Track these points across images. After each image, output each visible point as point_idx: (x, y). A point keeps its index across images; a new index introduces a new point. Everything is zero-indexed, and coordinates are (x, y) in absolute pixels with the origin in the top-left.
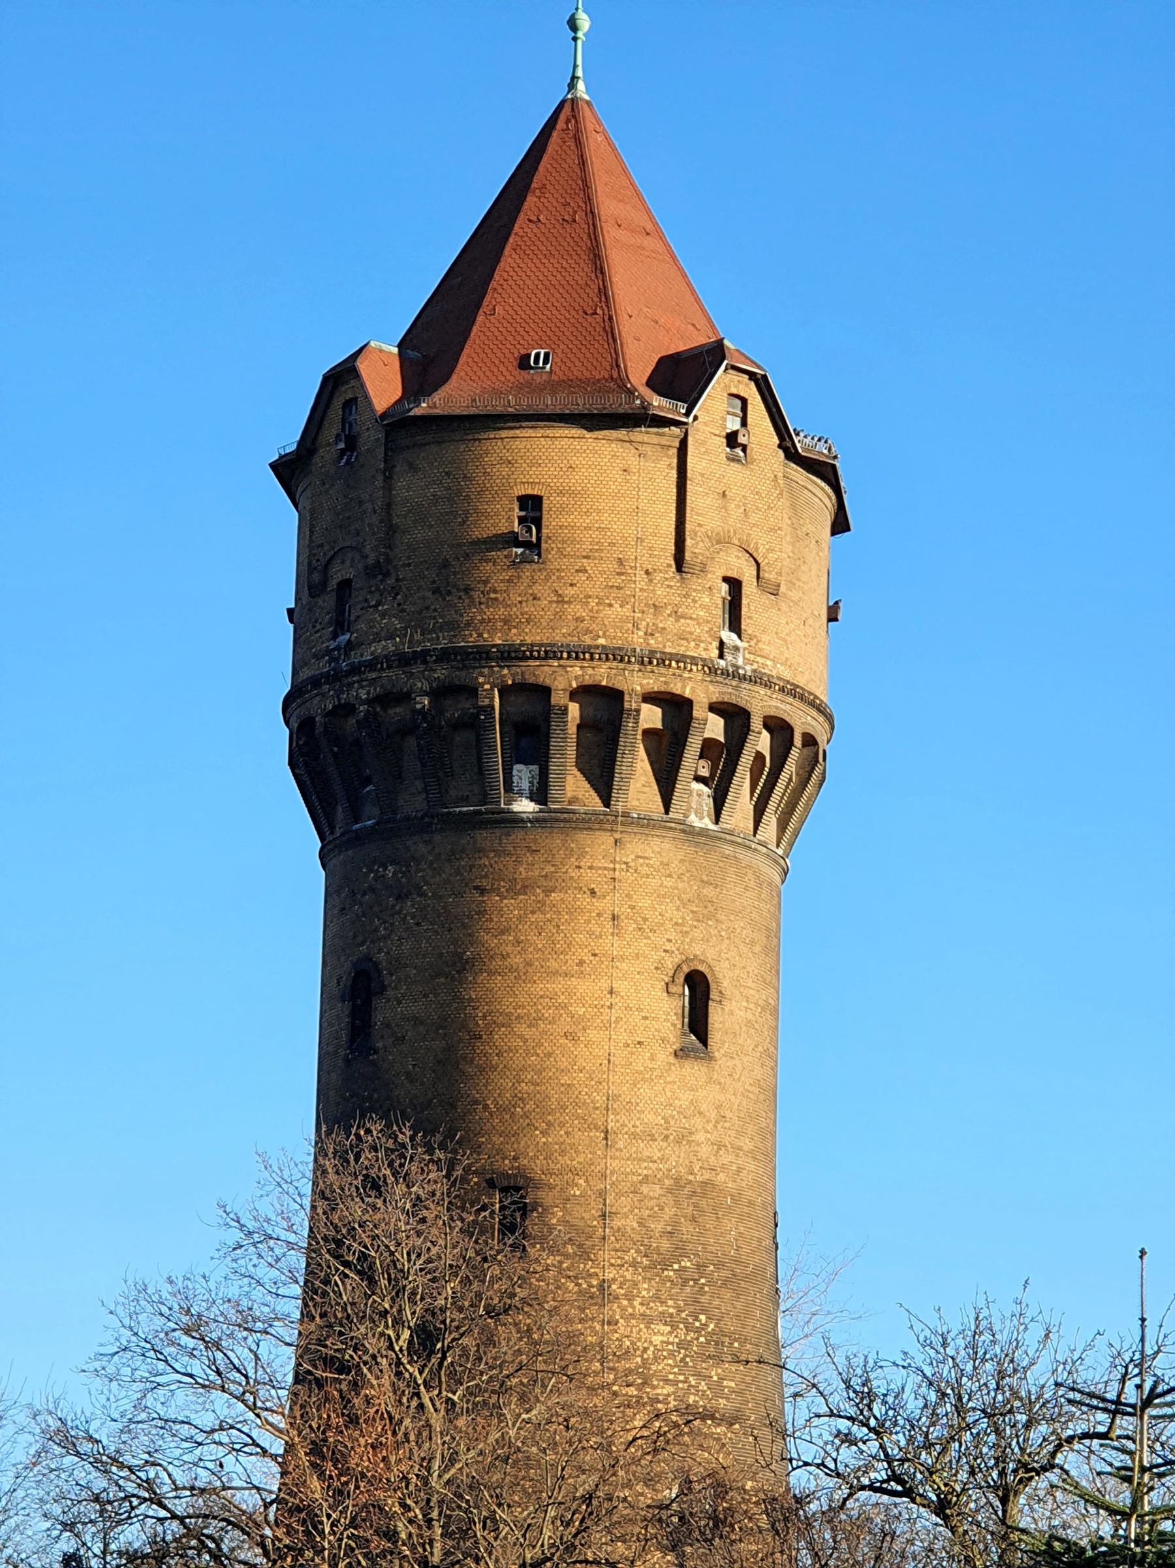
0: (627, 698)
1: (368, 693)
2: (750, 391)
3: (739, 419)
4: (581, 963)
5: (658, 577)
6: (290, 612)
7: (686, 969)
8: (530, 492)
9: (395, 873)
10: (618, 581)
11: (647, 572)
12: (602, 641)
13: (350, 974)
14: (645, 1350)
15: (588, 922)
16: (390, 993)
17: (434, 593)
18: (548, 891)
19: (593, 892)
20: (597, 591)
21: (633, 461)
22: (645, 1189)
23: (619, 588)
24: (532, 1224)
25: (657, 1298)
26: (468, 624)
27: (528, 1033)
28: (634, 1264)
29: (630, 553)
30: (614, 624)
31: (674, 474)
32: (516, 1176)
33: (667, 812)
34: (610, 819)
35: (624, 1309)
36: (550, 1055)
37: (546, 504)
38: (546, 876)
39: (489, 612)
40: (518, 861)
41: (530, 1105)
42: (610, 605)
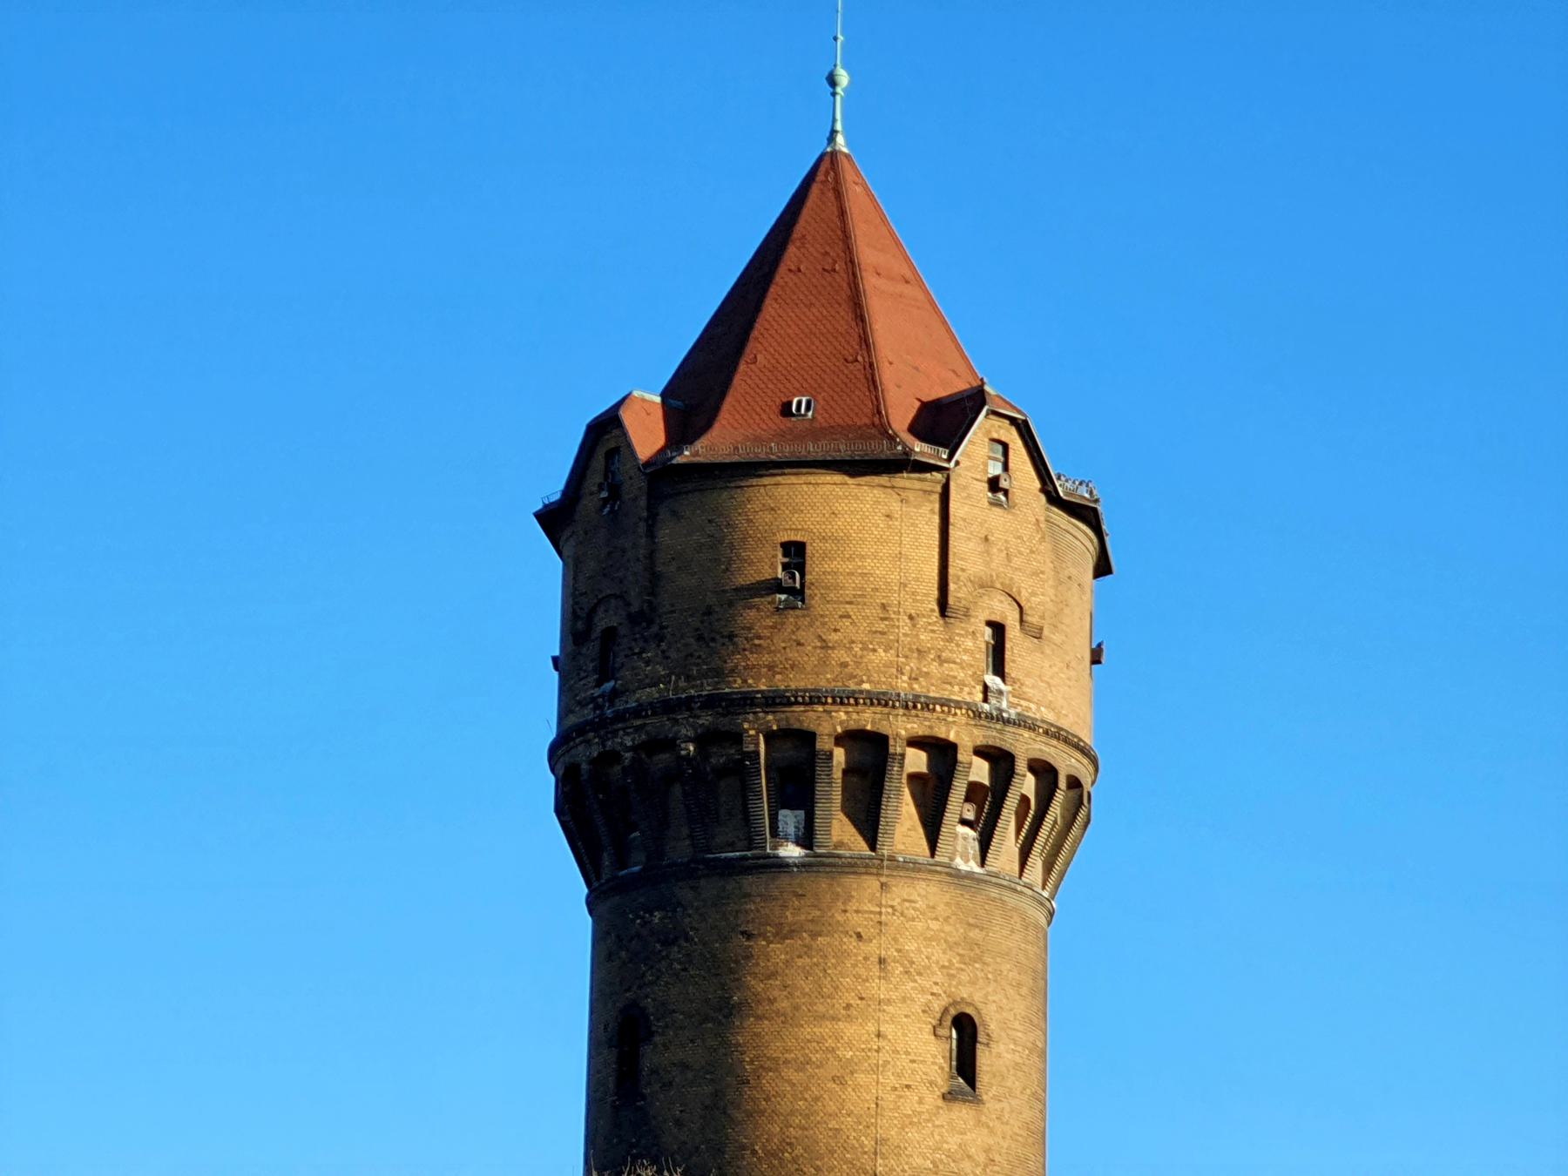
0: (891, 742)
3: (936, 497)
4: (848, 1006)
5: (922, 622)
6: (555, 660)
7: (953, 1012)
10: (882, 626)
11: (911, 617)
12: (866, 686)
15: (855, 966)
16: (657, 1039)
18: (815, 935)
19: (859, 936)
27: (795, 1077)
31: (936, 519)
33: (933, 855)
36: (816, 1099)
37: (809, 550)
40: (784, 907)
41: (799, 1150)
42: (874, 650)
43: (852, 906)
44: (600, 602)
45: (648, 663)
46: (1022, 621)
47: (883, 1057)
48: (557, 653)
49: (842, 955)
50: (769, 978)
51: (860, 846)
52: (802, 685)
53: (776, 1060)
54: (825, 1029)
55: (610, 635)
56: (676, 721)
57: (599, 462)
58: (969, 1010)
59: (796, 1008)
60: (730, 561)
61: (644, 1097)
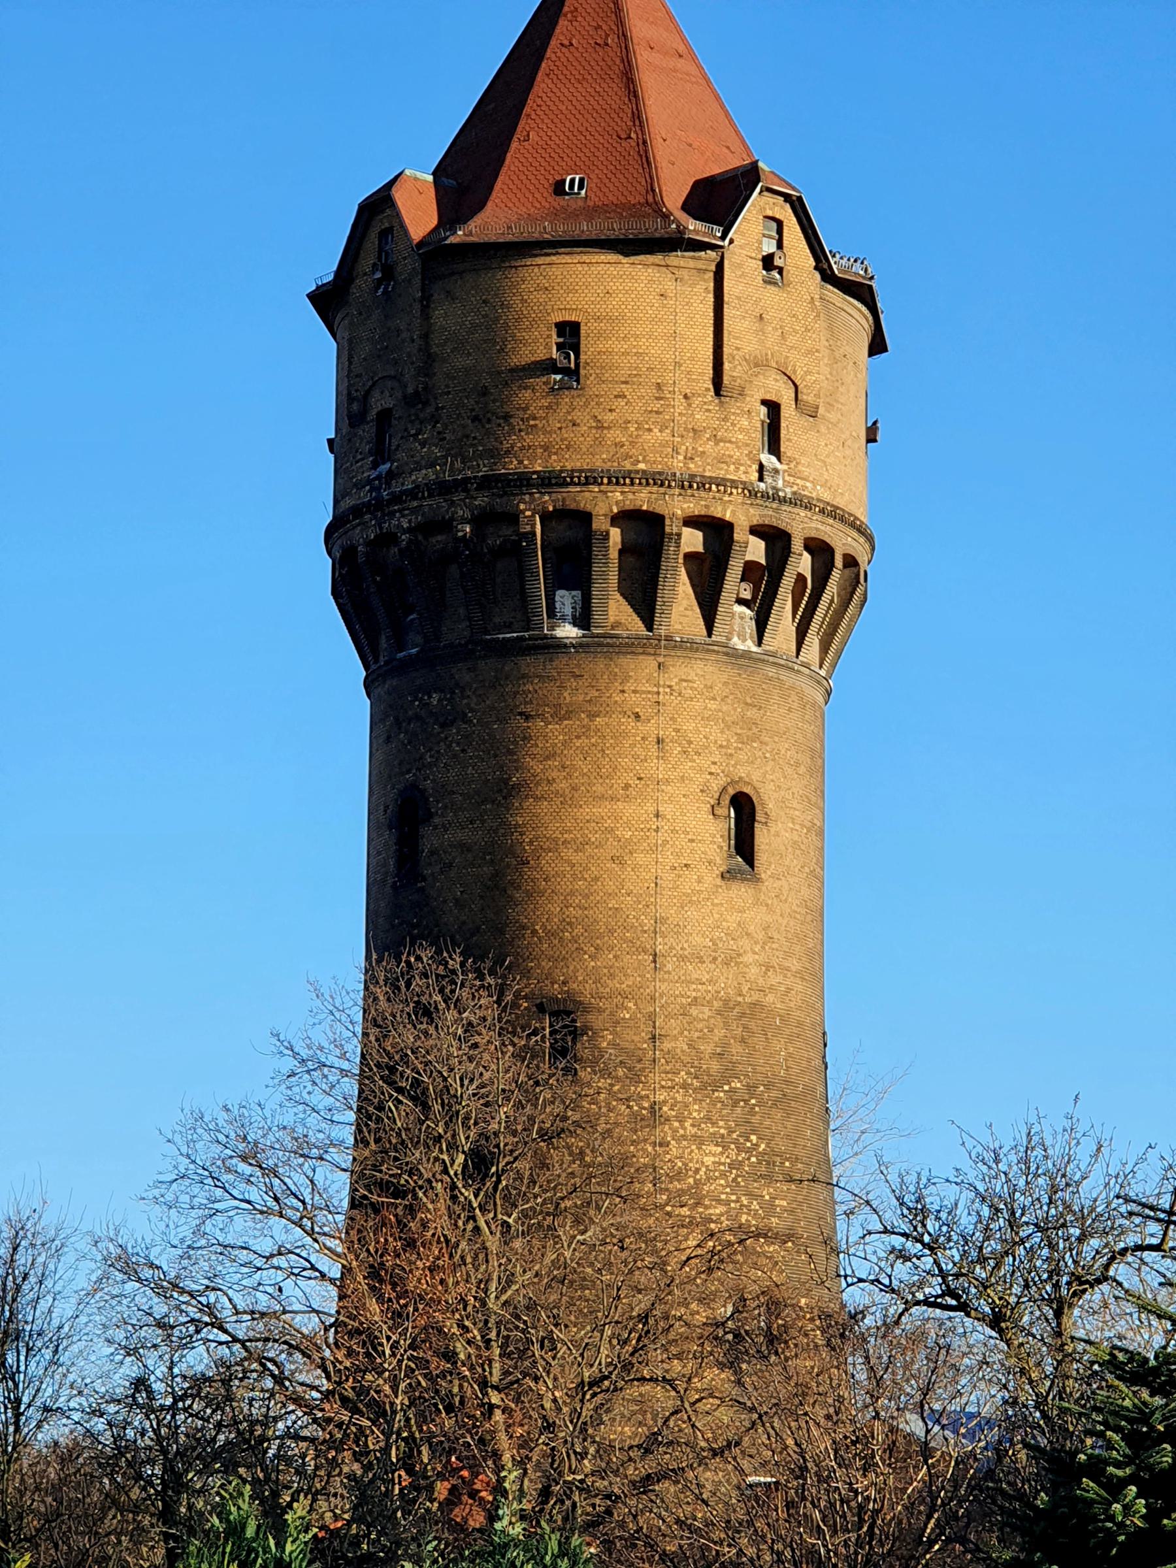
0: (667, 522)
1: (410, 522)
3: (775, 242)
4: (627, 787)
5: (697, 401)
6: (331, 442)
8: (567, 318)
10: (657, 406)
11: (686, 397)
12: (642, 466)
14: (697, 1171)
15: (633, 746)
18: (592, 716)
19: (637, 716)
23: (657, 412)
24: (583, 1048)
26: (508, 452)
27: (576, 858)
28: (685, 1086)
29: (669, 378)
30: (655, 448)
33: (710, 635)
35: (675, 1131)
36: (596, 879)
41: (579, 930)
42: (650, 430)
45: (423, 444)
50: (548, 758)
51: (636, 625)
58: (747, 790)
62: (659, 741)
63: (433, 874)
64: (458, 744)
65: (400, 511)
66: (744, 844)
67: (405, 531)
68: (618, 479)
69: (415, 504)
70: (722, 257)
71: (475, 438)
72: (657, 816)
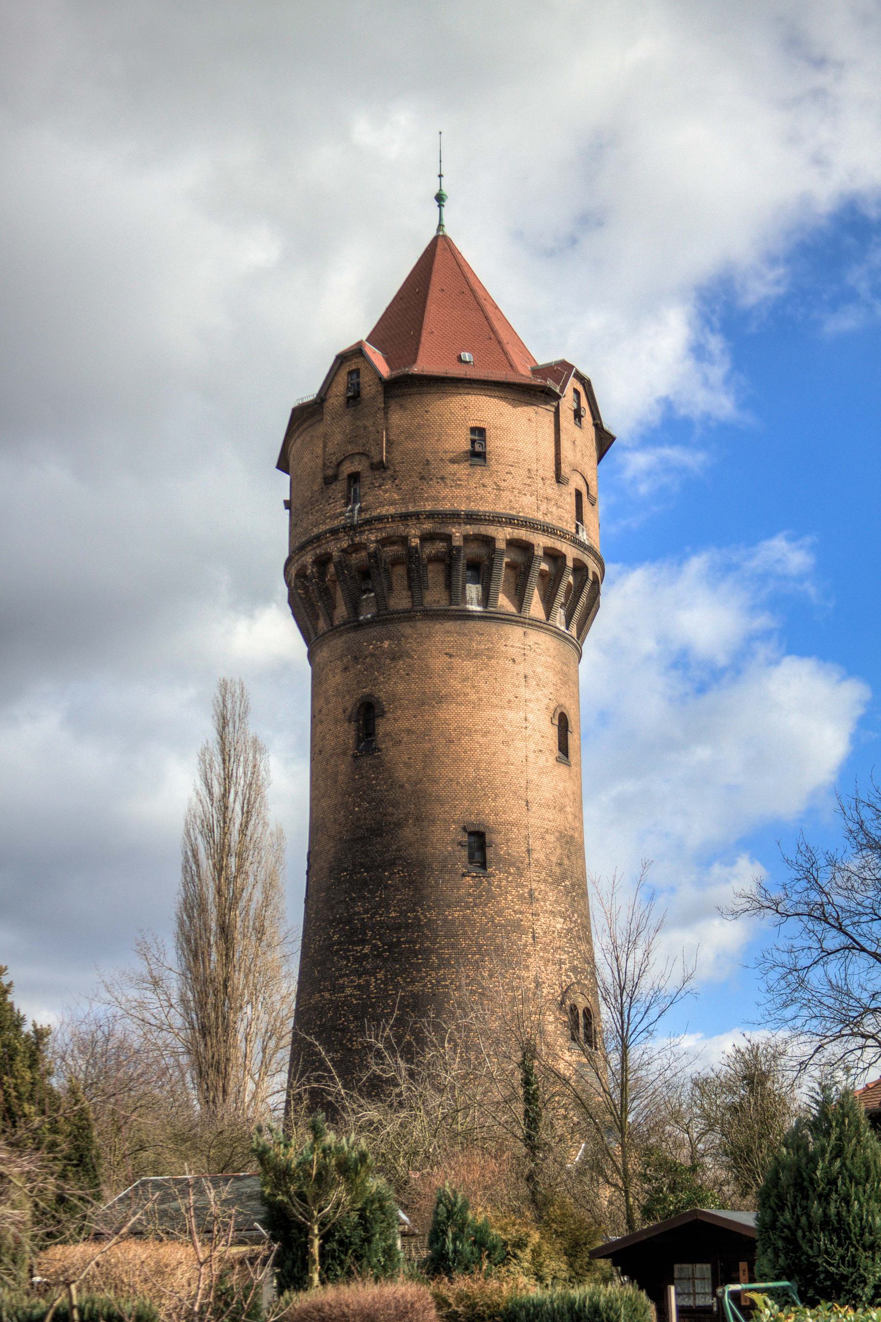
0: (536, 548)
1: (376, 537)
2: (580, 389)
3: (552, 414)
4: (509, 701)
5: (548, 482)
6: (286, 502)
7: (559, 711)
8: (478, 425)
9: (389, 645)
10: (528, 481)
11: (543, 479)
12: (521, 514)
13: (356, 704)
14: (554, 932)
15: (512, 678)
16: (389, 715)
17: (421, 479)
18: (490, 658)
19: (514, 661)
20: (518, 486)
21: (533, 415)
22: (547, 836)
23: (529, 485)
24: (490, 854)
25: (556, 901)
26: (444, 498)
27: (482, 740)
28: (545, 881)
29: (534, 467)
30: (527, 505)
31: (552, 426)
32: (479, 824)
33: (548, 619)
34: (519, 620)
35: (542, 907)
36: (494, 754)
37: (488, 433)
38: (488, 649)
39: (457, 492)
40: (471, 640)
41: (485, 783)
42: (525, 494)
43: (509, 643)
44: (346, 458)
45: (386, 492)
46: (588, 493)
47: (529, 732)
48: (288, 498)
49: (505, 671)
50: (464, 680)
51: (512, 609)
52: (487, 509)
53: (470, 730)
54: (497, 713)
55: (354, 478)
56: (408, 525)
57: (342, 377)
58: (565, 712)
59: (480, 700)
60: (440, 434)
61: (380, 750)
62: (525, 677)
63: (386, 748)
64: (404, 670)
65: (368, 530)
66: (563, 747)
67: (372, 542)
68: (511, 521)
69: (381, 526)
70: (558, 404)
71: (422, 489)
72: (526, 720)
